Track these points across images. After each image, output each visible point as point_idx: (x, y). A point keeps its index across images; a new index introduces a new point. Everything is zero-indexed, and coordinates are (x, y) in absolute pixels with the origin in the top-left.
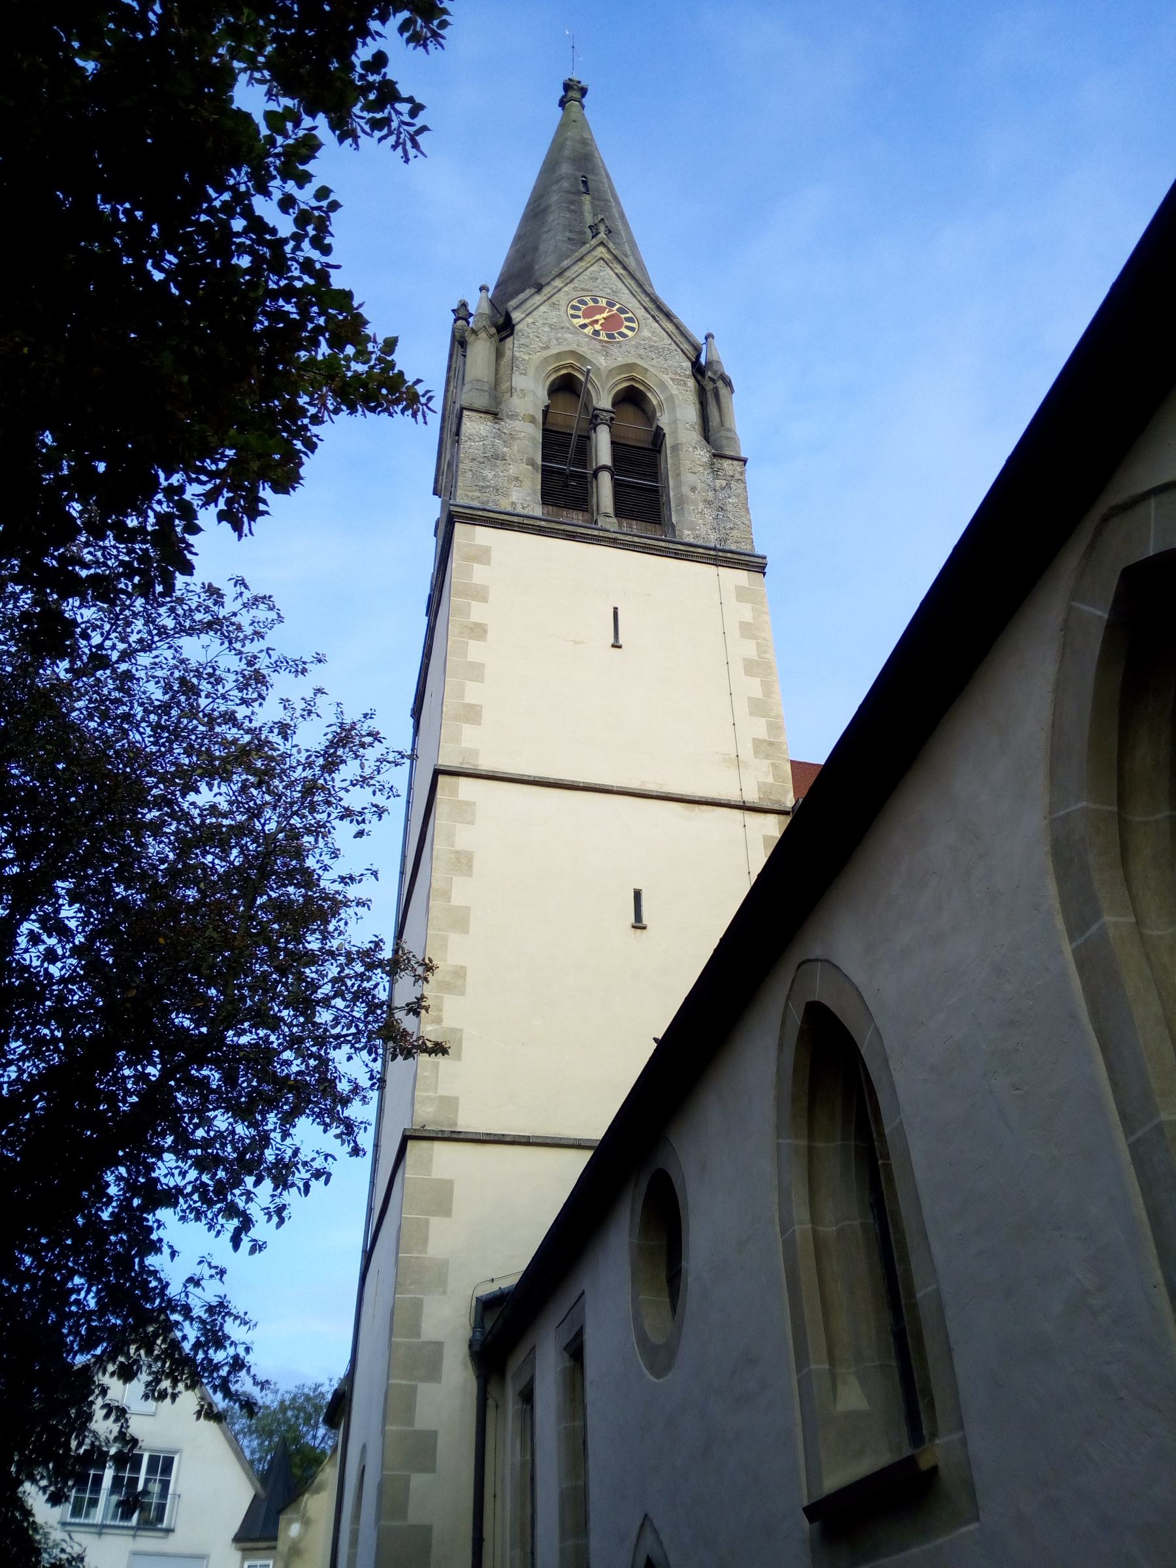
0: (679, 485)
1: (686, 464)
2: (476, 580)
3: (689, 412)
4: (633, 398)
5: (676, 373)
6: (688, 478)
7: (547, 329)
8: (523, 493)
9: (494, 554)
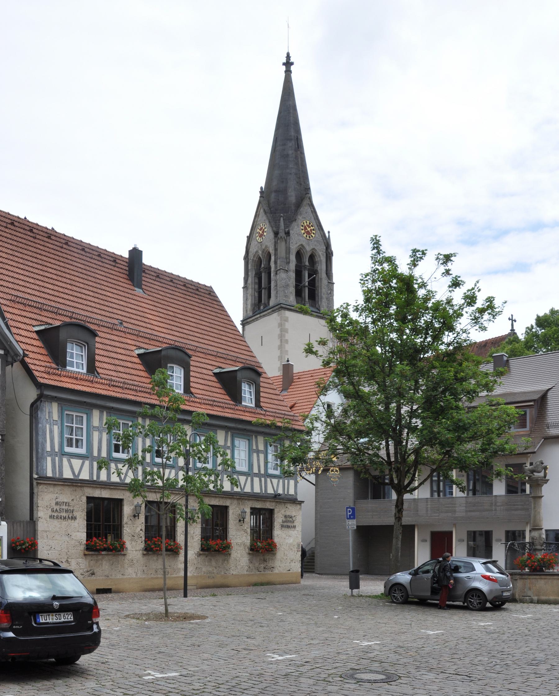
1: (323, 285)
4: (312, 258)
6: (324, 290)
8: (292, 299)
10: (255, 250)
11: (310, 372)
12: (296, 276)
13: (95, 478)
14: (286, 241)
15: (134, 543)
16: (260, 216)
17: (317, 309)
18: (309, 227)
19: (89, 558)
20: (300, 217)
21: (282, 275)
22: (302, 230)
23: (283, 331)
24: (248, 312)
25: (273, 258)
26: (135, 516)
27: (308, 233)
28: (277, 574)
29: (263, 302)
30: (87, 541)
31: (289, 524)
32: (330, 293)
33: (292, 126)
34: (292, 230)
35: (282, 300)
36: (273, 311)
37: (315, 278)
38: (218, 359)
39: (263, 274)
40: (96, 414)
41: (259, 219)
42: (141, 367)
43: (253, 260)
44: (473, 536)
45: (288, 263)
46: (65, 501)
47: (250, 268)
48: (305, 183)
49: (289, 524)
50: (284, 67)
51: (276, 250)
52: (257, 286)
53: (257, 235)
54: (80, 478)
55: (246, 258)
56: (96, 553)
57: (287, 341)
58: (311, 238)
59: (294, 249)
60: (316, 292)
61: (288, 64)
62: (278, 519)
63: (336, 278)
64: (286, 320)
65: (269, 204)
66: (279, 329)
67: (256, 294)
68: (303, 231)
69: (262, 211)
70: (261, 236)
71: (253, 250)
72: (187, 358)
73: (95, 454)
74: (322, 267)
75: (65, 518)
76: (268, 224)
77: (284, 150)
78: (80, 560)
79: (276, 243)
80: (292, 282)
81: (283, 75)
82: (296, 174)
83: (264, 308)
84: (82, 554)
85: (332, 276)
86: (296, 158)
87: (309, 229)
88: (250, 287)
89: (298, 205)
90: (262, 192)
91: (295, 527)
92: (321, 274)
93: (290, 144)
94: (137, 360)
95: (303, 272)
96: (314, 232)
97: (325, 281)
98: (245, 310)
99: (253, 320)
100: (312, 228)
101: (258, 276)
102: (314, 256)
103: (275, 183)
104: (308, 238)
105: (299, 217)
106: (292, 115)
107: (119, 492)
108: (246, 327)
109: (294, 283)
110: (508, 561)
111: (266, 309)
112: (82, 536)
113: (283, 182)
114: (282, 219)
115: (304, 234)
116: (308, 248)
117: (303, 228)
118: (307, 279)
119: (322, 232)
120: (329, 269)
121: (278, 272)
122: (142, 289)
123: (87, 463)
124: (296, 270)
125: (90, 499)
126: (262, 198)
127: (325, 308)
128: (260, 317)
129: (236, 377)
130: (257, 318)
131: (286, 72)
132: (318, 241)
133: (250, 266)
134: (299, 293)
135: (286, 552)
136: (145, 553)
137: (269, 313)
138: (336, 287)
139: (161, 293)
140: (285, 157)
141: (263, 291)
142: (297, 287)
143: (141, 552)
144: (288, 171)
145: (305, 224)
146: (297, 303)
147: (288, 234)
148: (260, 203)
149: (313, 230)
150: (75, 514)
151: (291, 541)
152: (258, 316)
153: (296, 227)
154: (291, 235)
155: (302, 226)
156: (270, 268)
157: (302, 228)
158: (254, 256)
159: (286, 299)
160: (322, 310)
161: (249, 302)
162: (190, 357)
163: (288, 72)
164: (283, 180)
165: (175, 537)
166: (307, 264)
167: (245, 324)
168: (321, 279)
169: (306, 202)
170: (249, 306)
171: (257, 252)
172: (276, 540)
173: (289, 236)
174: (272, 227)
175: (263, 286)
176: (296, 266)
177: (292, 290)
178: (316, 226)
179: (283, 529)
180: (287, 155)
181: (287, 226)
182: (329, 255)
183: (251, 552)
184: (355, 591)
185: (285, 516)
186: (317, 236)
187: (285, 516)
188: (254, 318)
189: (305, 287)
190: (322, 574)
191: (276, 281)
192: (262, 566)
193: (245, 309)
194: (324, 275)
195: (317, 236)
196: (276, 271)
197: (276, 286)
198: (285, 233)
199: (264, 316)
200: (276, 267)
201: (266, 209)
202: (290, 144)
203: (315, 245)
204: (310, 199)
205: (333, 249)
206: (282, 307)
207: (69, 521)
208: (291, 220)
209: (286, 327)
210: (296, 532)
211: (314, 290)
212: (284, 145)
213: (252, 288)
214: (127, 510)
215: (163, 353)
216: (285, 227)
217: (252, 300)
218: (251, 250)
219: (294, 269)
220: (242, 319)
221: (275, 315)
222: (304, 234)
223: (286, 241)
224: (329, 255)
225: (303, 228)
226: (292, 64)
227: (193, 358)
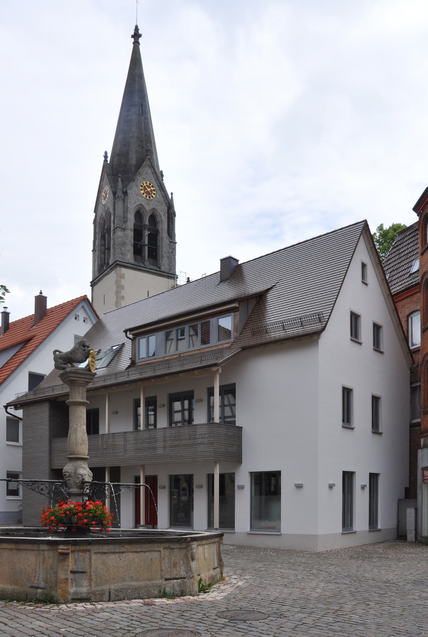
0: (162, 252)
1: (164, 244)
2: (122, 273)
3: (165, 226)
4: (153, 218)
5: (164, 212)
6: (164, 249)
7: (135, 195)
8: (130, 257)
9: (125, 276)
10: (101, 213)
12: (134, 235)
18: (149, 188)
21: (119, 233)
22: (142, 190)
23: (119, 287)
27: (148, 193)
32: (172, 252)
36: (111, 269)
43: (99, 223)
44: (175, 481)
45: (125, 222)
47: (97, 231)
51: (114, 209)
58: (152, 198)
59: (132, 207)
61: (136, 36)
63: (178, 238)
64: (122, 276)
66: (115, 286)
74: (163, 227)
81: (132, 46)
82: (138, 137)
83: (106, 267)
87: (149, 190)
89: (139, 166)
95: (144, 231)
96: (155, 192)
98: (94, 272)
100: (152, 188)
101: (103, 237)
104: (148, 198)
108: (94, 288)
109: (132, 241)
110: (253, 511)
114: (120, 179)
115: (143, 194)
116: (148, 208)
117: (142, 188)
119: (163, 193)
120: (171, 229)
130: (101, 278)
132: (159, 202)
133: (97, 229)
134: (138, 251)
138: (178, 247)
142: (135, 246)
145: (145, 184)
146: (135, 260)
147: (125, 193)
149: (154, 190)
154: (129, 195)
155: (142, 186)
157: (141, 188)
158: (100, 219)
159: (123, 257)
160: (163, 269)
163: (136, 44)
168: (162, 238)
169: (147, 163)
171: (102, 214)
173: (127, 195)
178: (157, 187)
181: (125, 186)
186: (158, 196)
189: (145, 245)
195: (158, 196)
198: (123, 193)
199: (106, 275)
200: (114, 226)
202: (134, 110)
203: (156, 205)
206: (117, 265)
219: (133, 228)
222: (143, 194)
224: (171, 215)
225: (142, 188)
226: (140, 36)
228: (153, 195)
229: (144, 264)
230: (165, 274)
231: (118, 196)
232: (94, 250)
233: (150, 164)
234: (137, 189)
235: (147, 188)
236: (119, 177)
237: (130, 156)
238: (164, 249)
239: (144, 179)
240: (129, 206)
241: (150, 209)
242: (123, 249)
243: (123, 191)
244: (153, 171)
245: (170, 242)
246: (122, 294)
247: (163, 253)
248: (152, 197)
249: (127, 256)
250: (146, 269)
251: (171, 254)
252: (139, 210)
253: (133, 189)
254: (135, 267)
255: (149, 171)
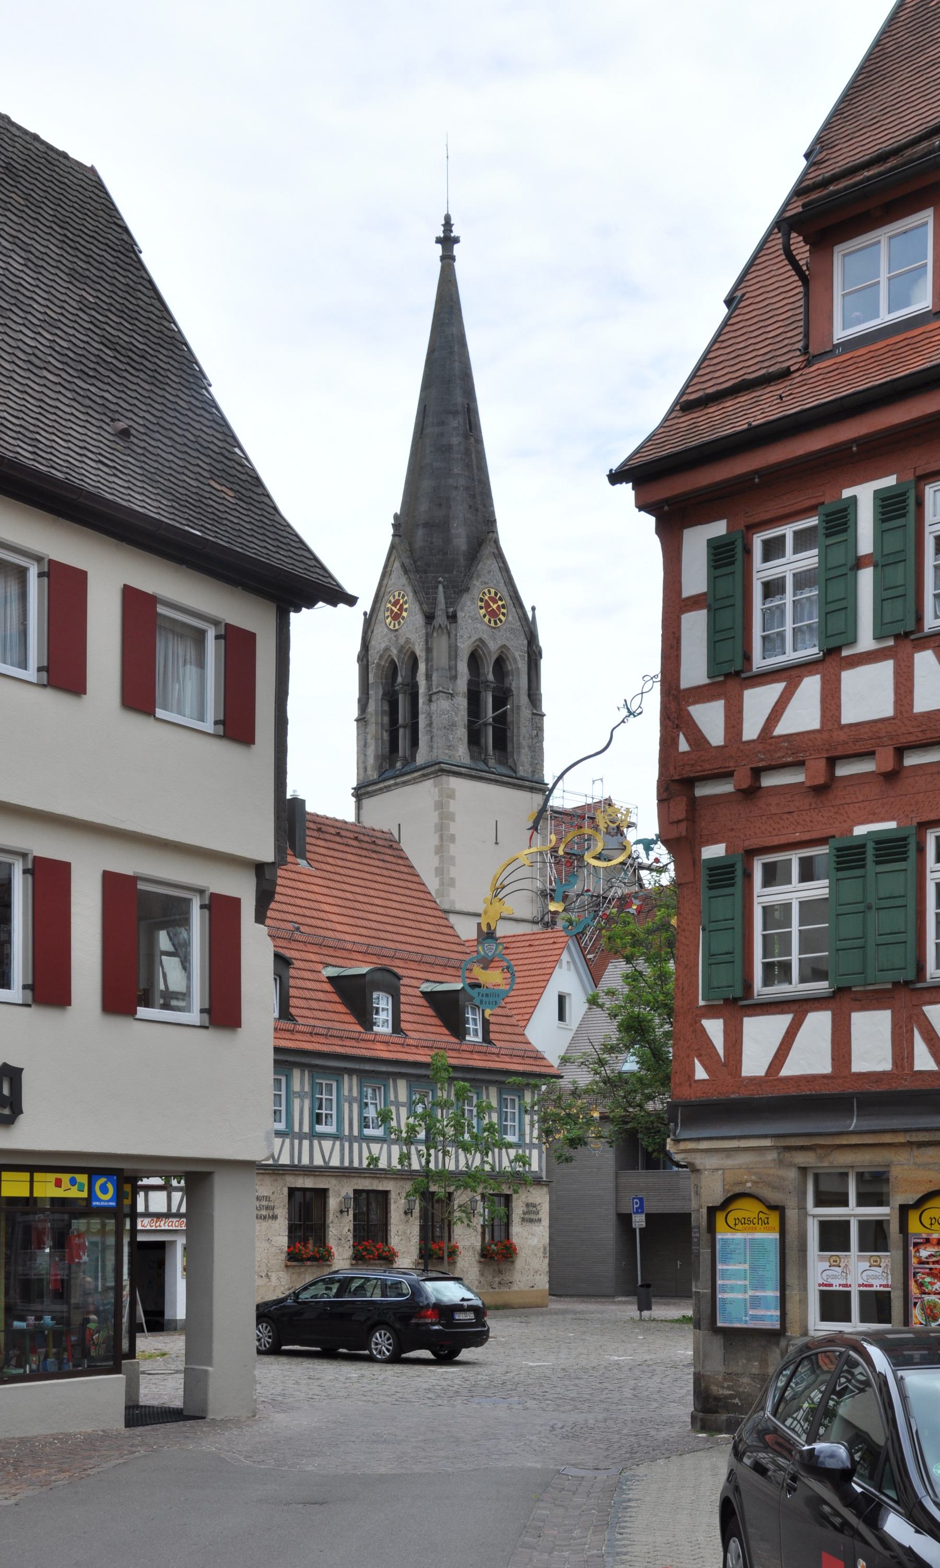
4: (500, 664)
5: (521, 651)
6: (523, 731)
8: (462, 753)
9: (457, 793)
10: (383, 646)
11: (528, 938)
12: (469, 704)
13: (296, 1163)
14: (449, 633)
15: (340, 1249)
16: (393, 576)
17: (510, 767)
18: (495, 602)
19: (291, 1270)
20: (476, 583)
21: (443, 704)
22: (481, 608)
23: (445, 817)
24: (369, 772)
25: (422, 667)
26: (342, 1212)
27: (493, 614)
28: (516, 1292)
29: (401, 753)
30: (289, 1247)
31: (532, 1216)
32: (537, 735)
33: (458, 381)
34: (462, 610)
35: (440, 754)
37: (505, 712)
38: (423, 967)
39: (401, 697)
40: (296, 1073)
41: (390, 583)
42: (335, 998)
43: (378, 665)
45: (454, 678)
46: (266, 1194)
47: (371, 680)
48: (484, 506)
49: (532, 1216)
50: (439, 247)
51: (429, 650)
52: (386, 719)
53: (388, 614)
54: (280, 1162)
55: (364, 658)
56: (299, 1264)
57: (452, 838)
59: (465, 648)
60: (509, 734)
61: (448, 241)
62: (518, 1208)
63: (547, 706)
64: (451, 795)
65: (412, 551)
67: (386, 736)
68: (483, 612)
69: (397, 565)
70: (396, 617)
71: (379, 643)
72: (395, 980)
73: (297, 1129)
74: (520, 684)
75: (265, 1217)
76: (411, 594)
77: (442, 435)
78: (281, 1274)
79: (428, 637)
80: (462, 717)
82: (467, 488)
84: (283, 1265)
85: (540, 701)
86: (467, 452)
87: (494, 606)
88: (372, 719)
90: (396, 526)
91: (540, 1220)
92: (518, 695)
93: (455, 424)
94: (328, 987)
95: (483, 694)
97: (526, 712)
99: (381, 789)
100: (500, 603)
102: (504, 661)
103: (424, 507)
104: (492, 624)
105: (475, 582)
106: (457, 358)
107: (324, 1179)
109: (466, 718)
111: (406, 769)
112: (282, 1241)
113: (440, 505)
114: (441, 588)
115: (485, 616)
116: (493, 646)
117: (483, 604)
118: (490, 713)
119: (519, 611)
121: (434, 698)
122: (306, 859)
123: (287, 1141)
124: (469, 690)
125: (292, 1191)
126: (397, 538)
127: (527, 766)
128: (396, 784)
129: (457, 1001)
130: (390, 786)
131: (442, 258)
132: (512, 630)
133: (371, 676)
134: (474, 738)
135: (528, 1259)
136: (354, 1262)
137: (414, 779)
138: (547, 721)
139: (330, 860)
140: (444, 450)
141: (401, 731)
143: (349, 1261)
144: (451, 481)
147: (453, 618)
148: (393, 547)
149: (503, 606)
150: (277, 1211)
151: (534, 1241)
152: (392, 782)
153: (469, 603)
154: (460, 621)
155: (481, 600)
156: (415, 686)
157: (480, 604)
158: (381, 657)
159: (450, 753)
160: (521, 773)
161: (371, 751)
162: (399, 978)
163: (448, 259)
164: (441, 501)
165: (387, 1239)
166: (491, 677)
167: (361, 795)
168: (518, 707)
169: (488, 550)
170: (371, 761)
171: (387, 649)
172: (515, 1240)
173: (456, 622)
174: (421, 604)
175: (401, 721)
176: (470, 683)
177: (462, 733)
179: (524, 1224)
180: (448, 448)
181: (452, 601)
182: (533, 657)
183: (482, 1260)
184: (646, 1313)
185: (527, 1205)
186: (510, 618)
187: (527, 1205)
188: (382, 785)
189: (486, 724)
190: (560, 1296)
191: (429, 716)
192: (497, 1279)
193: (362, 766)
194: (524, 700)
196: (430, 696)
197: (430, 725)
198: (448, 617)
199: (405, 783)
200: (429, 687)
201: (407, 562)
202: (455, 424)
203: (507, 638)
204: (496, 542)
205: (541, 644)
206: (442, 770)
207: (270, 1221)
208: (458, 589)
209: (452, 809)
210: (541, 1228)
211: (505, 731)
212: (442, 423)
213: (377, 724)
214: (333, 1203)
215: (368, 978)
216: (446, 604)
217: (376, 747)
218: (373, 643)
219: (466, 690)
220: (355, 785)
221: (428, 784)
222: (485, 616)
223: (449, 633)
224: (534, 656)
225: (483, 604)
226: (456, 240)
227: (404, 981)
228: (501, 616)
229: (486, 764)
230: (527, 783)
231: (440, 626)
232: (362, 720)
233: (496, 551)
234: (472, 607)
235: (491, 604)
236: (440, 582)
237: (453, 531)
238: (523, 731)
239: (486, 583)
240: (459, 644)
241: (497, 647)
242: (451, 737)
243: (447, 612)
244: (501, 565)
245: (534, 714)
246: (452, 832)
247: (521, 738)
248: (501, 621)
249: (458, 751)
250: (492, 776)
251: (535, 741)
252: (476, 650)
253: (466, 608)
254: (473, 773)
255: (493, 565)
